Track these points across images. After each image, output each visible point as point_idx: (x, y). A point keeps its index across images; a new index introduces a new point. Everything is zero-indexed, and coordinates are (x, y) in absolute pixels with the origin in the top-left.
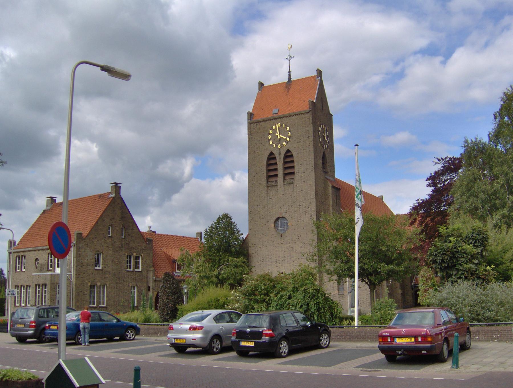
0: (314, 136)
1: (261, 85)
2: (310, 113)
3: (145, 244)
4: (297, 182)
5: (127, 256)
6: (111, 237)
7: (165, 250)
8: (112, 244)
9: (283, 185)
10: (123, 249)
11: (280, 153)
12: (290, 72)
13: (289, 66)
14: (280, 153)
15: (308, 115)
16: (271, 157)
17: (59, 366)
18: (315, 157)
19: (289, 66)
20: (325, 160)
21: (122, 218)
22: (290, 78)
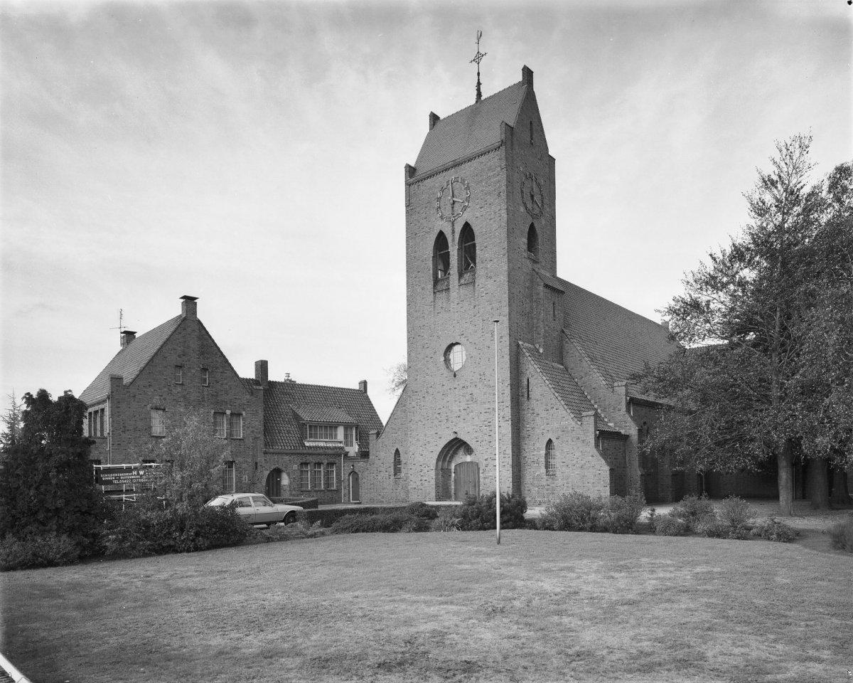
0: (508, 192)
1: (434, 118)
2: (503, 148)
3: (248, 397)
4: (480, 281)
5: (464, 423)
6: (182, 384)
7: (295, 408)
8: (184, 397)
9: (457, 287)
10: (206, 405)
11: (453, 232)
12: (479, 84)
13: (479, 74)
14: (453, 232)
15: (497, 153)
16: (441, 240)
17: (502, 528)
18: (510, 233)
19: (479, 74)
20: (535, 235)
21: (202, 353)
22: (479, 94)
